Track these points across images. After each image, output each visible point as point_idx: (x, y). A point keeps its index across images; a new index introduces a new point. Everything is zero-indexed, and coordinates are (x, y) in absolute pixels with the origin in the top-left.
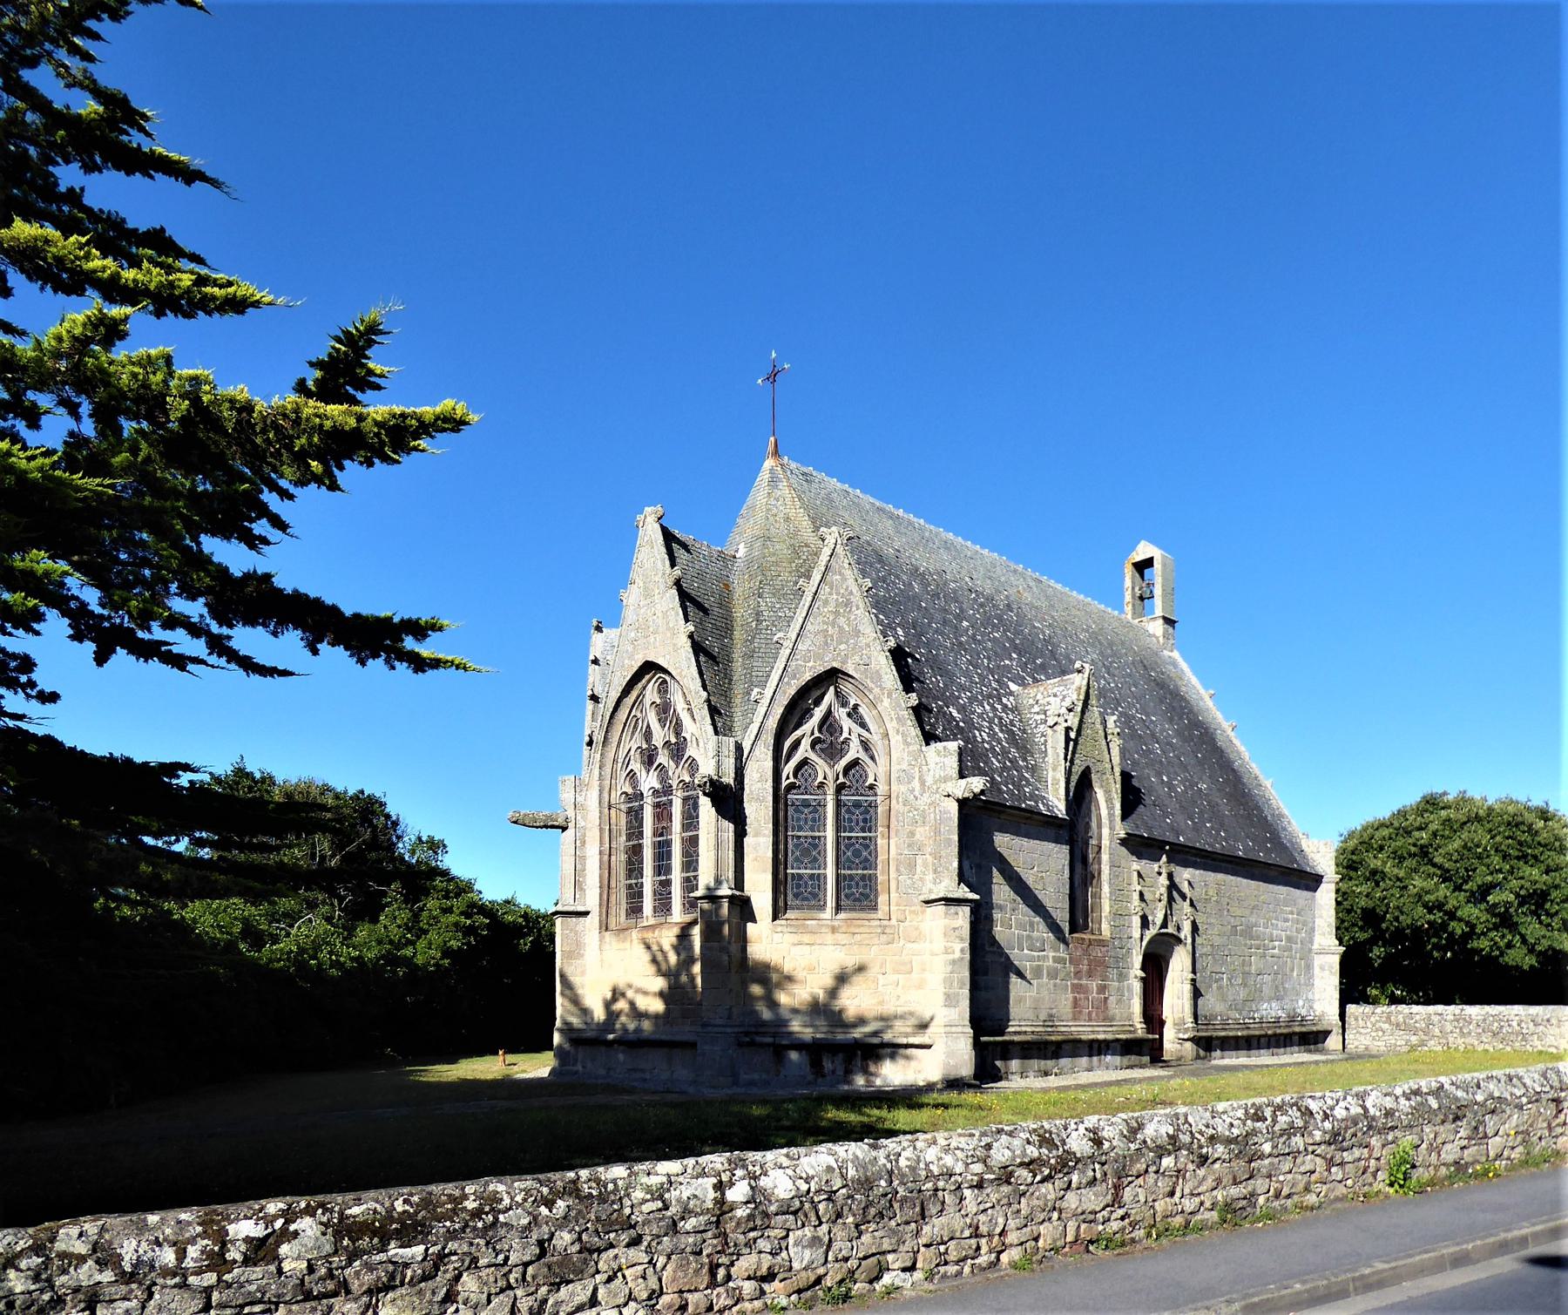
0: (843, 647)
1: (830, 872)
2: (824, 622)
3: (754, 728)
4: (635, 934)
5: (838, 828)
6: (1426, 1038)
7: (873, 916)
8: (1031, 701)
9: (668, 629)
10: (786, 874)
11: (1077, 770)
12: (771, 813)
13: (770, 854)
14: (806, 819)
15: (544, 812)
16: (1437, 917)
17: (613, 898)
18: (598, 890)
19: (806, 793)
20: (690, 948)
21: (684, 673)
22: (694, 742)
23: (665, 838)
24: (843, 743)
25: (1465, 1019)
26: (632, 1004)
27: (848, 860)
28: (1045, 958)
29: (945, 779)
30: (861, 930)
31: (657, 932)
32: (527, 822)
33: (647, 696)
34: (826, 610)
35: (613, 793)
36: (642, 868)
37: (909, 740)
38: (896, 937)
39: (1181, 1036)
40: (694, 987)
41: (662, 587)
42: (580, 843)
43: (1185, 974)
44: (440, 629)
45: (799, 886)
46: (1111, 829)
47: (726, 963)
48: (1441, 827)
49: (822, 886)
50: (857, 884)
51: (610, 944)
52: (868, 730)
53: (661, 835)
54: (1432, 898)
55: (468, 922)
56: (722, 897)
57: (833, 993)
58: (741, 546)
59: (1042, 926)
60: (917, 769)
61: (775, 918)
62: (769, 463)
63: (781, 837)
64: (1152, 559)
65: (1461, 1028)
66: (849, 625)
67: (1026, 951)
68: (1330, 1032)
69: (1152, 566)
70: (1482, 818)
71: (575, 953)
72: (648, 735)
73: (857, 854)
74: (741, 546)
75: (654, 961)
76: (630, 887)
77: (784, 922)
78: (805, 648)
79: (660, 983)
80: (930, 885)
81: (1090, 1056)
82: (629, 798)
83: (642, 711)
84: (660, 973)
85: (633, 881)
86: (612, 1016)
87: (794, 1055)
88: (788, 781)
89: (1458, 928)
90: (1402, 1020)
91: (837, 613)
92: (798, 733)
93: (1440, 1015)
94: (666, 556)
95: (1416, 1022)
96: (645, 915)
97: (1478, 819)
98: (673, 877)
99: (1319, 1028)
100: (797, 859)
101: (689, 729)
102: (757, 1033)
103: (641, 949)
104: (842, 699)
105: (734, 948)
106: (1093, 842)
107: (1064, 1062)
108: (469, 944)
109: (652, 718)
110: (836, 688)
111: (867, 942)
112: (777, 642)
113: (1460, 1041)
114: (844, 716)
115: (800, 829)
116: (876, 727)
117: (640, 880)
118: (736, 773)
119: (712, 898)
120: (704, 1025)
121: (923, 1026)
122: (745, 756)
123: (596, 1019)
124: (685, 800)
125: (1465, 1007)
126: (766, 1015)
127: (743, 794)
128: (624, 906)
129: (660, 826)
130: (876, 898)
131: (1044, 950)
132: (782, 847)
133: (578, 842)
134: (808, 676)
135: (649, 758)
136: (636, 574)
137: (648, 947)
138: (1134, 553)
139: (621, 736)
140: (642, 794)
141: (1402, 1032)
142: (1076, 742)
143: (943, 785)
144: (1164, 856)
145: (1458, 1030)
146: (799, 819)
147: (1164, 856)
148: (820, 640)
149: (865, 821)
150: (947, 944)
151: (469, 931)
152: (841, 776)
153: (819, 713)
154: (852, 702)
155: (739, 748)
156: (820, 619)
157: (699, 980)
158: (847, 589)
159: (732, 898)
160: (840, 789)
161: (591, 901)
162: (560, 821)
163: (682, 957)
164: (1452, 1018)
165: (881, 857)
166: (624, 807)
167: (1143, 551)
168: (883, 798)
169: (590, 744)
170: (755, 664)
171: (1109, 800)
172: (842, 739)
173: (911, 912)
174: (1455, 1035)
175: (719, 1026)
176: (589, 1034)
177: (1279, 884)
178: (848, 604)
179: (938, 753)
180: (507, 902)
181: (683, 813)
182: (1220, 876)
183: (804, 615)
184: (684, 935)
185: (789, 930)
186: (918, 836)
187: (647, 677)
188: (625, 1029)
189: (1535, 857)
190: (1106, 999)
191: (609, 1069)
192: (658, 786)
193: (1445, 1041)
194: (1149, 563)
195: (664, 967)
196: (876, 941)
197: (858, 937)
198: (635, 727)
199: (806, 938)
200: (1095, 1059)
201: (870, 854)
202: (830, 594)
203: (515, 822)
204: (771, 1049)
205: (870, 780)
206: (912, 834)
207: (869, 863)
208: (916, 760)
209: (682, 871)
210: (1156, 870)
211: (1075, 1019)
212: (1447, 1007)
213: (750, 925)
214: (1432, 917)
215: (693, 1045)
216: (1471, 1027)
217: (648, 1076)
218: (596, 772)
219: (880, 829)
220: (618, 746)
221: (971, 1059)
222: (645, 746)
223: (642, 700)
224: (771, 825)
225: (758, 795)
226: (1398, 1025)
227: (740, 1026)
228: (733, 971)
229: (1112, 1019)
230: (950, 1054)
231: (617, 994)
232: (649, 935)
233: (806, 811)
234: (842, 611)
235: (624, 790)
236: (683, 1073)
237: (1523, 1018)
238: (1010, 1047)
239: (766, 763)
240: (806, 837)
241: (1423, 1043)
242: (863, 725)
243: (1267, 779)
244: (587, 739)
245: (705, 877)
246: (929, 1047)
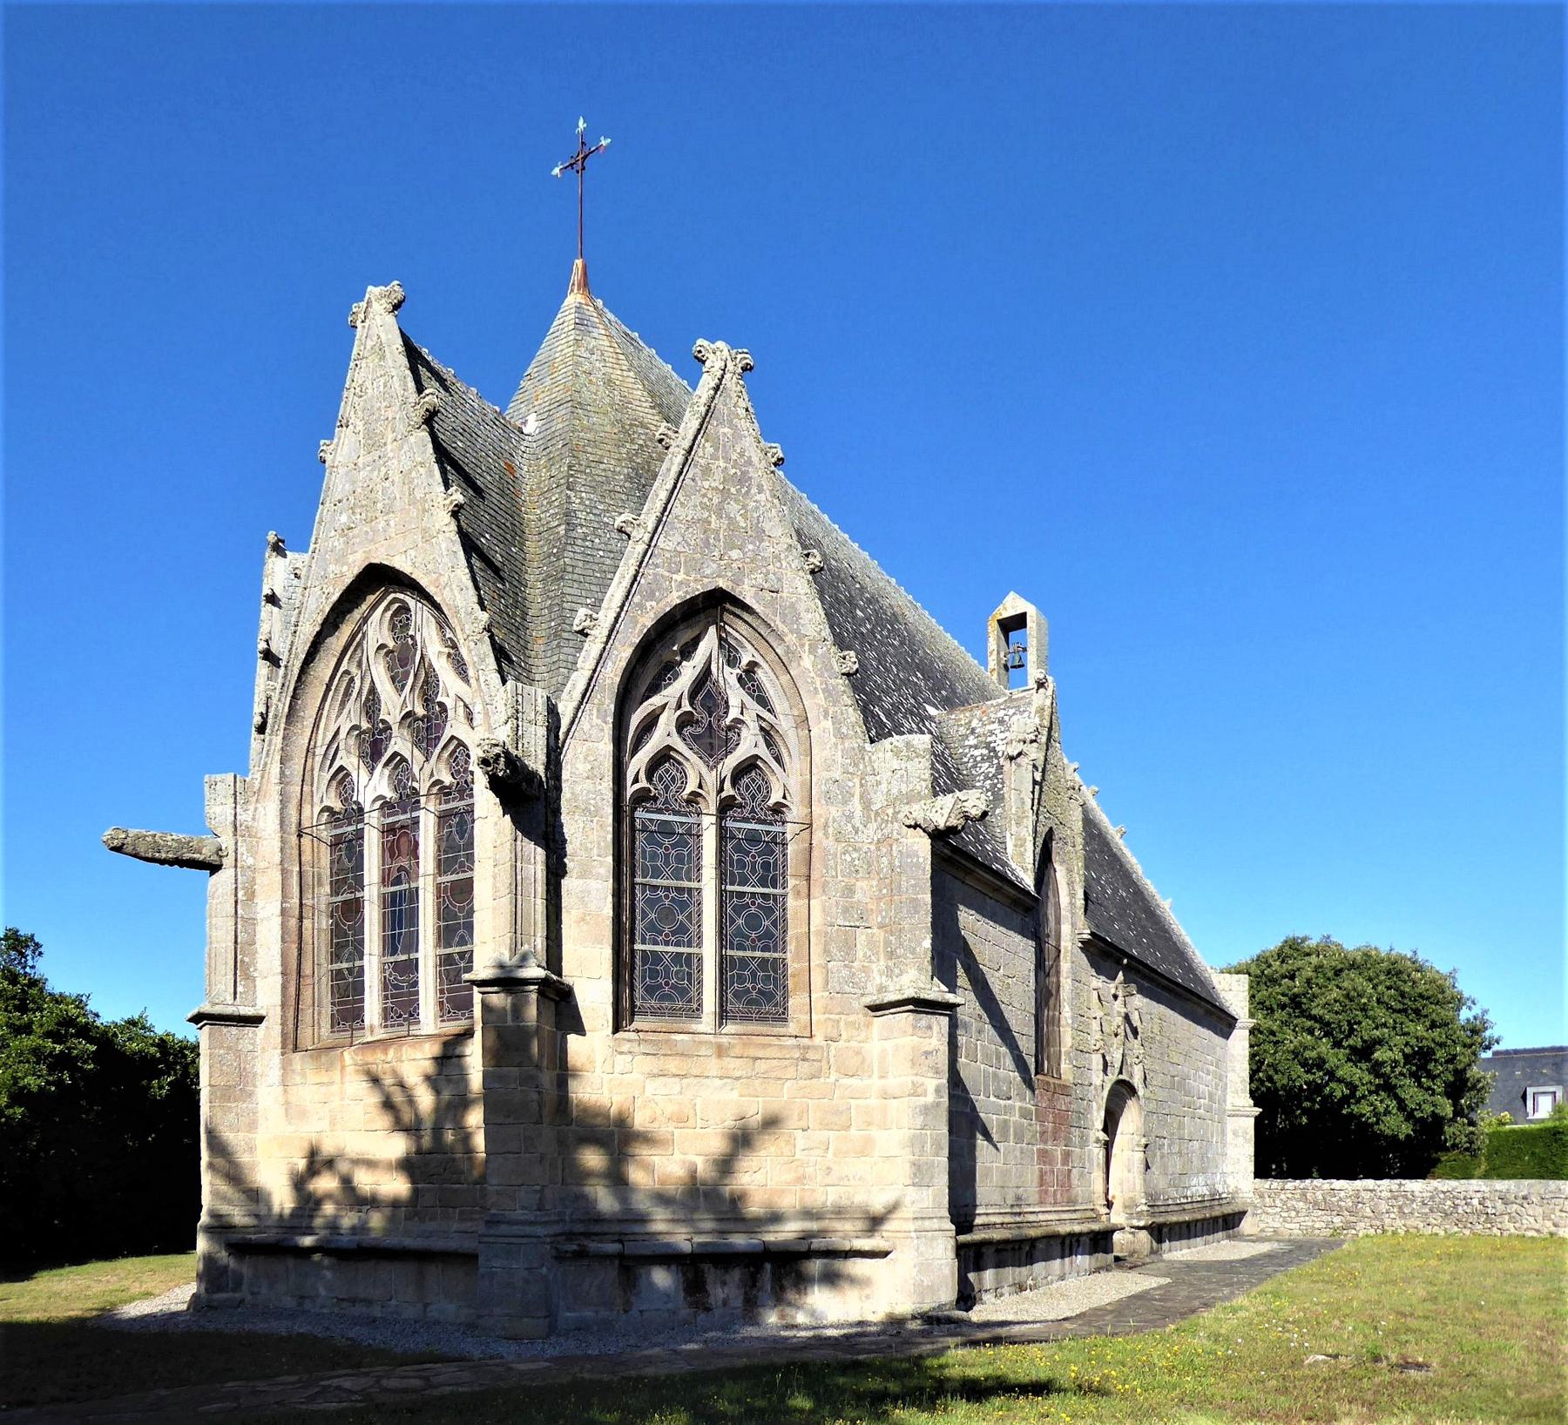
0: (735, 554)
1: (709, 951)
2: (704, 507)
3: (579, 680)
4: (348, 1056)
5: (722, 877)
6: (1353, 1219)
7: (782, 1031)
8: (962, 730)
9: (413, 503)
10: (633, 951)
11: (1043, 830)
12: (610, 837)
13: (608, 911)
14: (667, 856)
15: (173, 839)
16: (1318, 1076)
17: (307, 994)
18: (279, 979)
19: (667, 809)
20: (462, 1077)
21: (444, 580)
22: (461, 710)
23: (404, 886)
24: (729, 728)
25: (1405, 1197)
26: (347, 1182)
27: (739, 933)
28: (1008, 1110)
29: (910, 798)
30: (768, 1053)
31: (391, 1052)
32: (142, 850)
33: (370, 633)
34: (706, 484)
36: (362, 942)
37: (844, 730)
38: (825, 1067)
39: (1135, 1223)
40: (469, 1150)
41: (401, 428)
42: (243, 898)
43: (1137, 1138)
45: (654, 974)
46: (1072, 925)
47: (535, 1106)
48: (1314, 974)
49: (695, 976)
50: (754, 974)
51: (304, 1075)
52: (771, 711)
53: (398, 881)
54: (1314, 1054)
55: (58, 1048)
56: (527, 982)
57: (726, 1165)
58: (532, 418)
59: (1009, 1061)
60: (857, 780)
61: (617, 1028)
62: (574, 299)
63: (626, 884)
64: (1023, 616)
65: (1400, 1207)
66: (744, 516)
67: (992, 1098)
68: (1244, 1213)
69: (1025, 626)
70: (1362, 964)
71: (238, 1088)
72: (372, 704)
73: (753, 922)
74: (532, 418)
75: (388, 1105)
76: (338, 975)
77: (633, 1035)
78: (670, 546)
79: (397, 1146)
80: (878, 979)
81: (1062, 1257)
83: (359, 665)
84: (399, 1126)
85: (345, 965)
86: (308, 1203)
87: (661, 1278)
88: (637, 786)
89: (1339, 1091)
90: (1321, 1197)
91: (724, 492)
92: (656, 701)
93: (1371, 1191)
94: (408, 372)
95: (1341, 1199)
96: (367, 1022)
97: (1353, 966)
98: (420, 955)
99: (1228, 1210)
100: (651, 927)
101: (450, 685)
102: (587, 1235)
103: (358, 1087)
104: (731, 655)
105: (547, 1078)
106: (1052, 941)
107: (1039, 1267)
108: (59, 1083)
109: (380, 674)
110: (720, 629)
112: (620, 530)
113: (1399, 1223)
114: (733, 680)
115: (657, 873)
116: (786, 705)
117: (358, 963)
118: (548, 756)
119: (507, 982)
120: (493, 1222)
121: (875, 1222)
122: (563, 729)
123: (276, 1209)
124: (443, 818)
125: (1403, 1182)
126: (604, 1199)
127: (559, 798)
128: (327, 1010)
129: (396, 865)
130: (785, 998)
131: (1009, 1098)
132: (626, 901)
133: (240, 894)
134: (675, 598)
135: (373, 746)
136: (349, 408)
137: (375, 1080)
138: (1001, 607)
139: (321, 708)
140: (361, 810)
141: (1320, 1213)
142: (1040, 784)
143: (905, 809)
144: (1121, 973)
145: (1395, 1210)
146: (654, 856)
147: (1121, 973)
148: (695, 535)
149: (766, 866)
150: (915, 1079)
151: (61, 1062)
152: (727, 784)
153: (688, 672)
154: (745, 660)
155: (552, 711)
156: (696, 499)
157: (479, 1141)
158: (742, 454)
159: (543, 983)
160: (726, 806)
161: (267, 996)
162: (206, 854)
163: (446, 1096)
164: (1389, 1195)
165: (794, 930)
166: (326, 834)
167: (1013, 605)
168: (797, 828)
169: (261, 729)
170: (568, 590)
171: (1070, 884)
172: (728, 721)
173: (847, 1024)
174: (1392, 1216)
175: (524, 1223)
176: (269, 1236)
177: (1203, 1026)
178: (743, 479)
179: (896, 753)
180: (132, 1023)
181: (439, 840)
182: (1162, 1008)
183: (669, 486)
184: (449, 1057)
185: (644, 1048)
186: (858, 896)
187: (371, 599)
188: (333, 1226)
189: (1417, 1012)
190: (1070, 1171)
191: (303, 1297)
192: (389, 794)
193: (1378, 1223)
194: (1019, 621)
195: (407, 1116)
197: (762, 1066)
198: (347, 694)
199: (673, 1065)
200: (1067, 1260)
201: (774, 924)
203: (118, 849)
205: (776, 797)
206: (849, 891)
207: (773, 938)
208: (856, 765)
209: (438, 945)
210: (1113, 991)
211: (1041, 1203)
212: (1378, 1182)
213: (572, 1039)
214: (1311, 1077)
215: (470, 1258)
216: (1414, 1206)
217: (377, 1311)
218: (275, 769)
219: (791, 882)
220: (316, 725)
221: (953, 1274)
222: (365, 725)
223: (360, 644)
224: (610, 859)
225: (587, 802)
226: (1316, 1203)
227: (557, 1222)
228: (546, 1120)
229: (1074, 1202)
230: (923, 1267)
231: (317, 1162)
232: (381, 1061)
233: (667, 842)
234: (733, 490)
235: (325, 804)
236: (446, 1308)
237: (1487, 1195)
238: (984, 1250)
239: (601, 745)
240: (667, 889)
241: (1348, 1226)
242: (763, 701)
243: (1165, 899)
244: (257, 720)
245: (488, 954)
246: (884, 1254)
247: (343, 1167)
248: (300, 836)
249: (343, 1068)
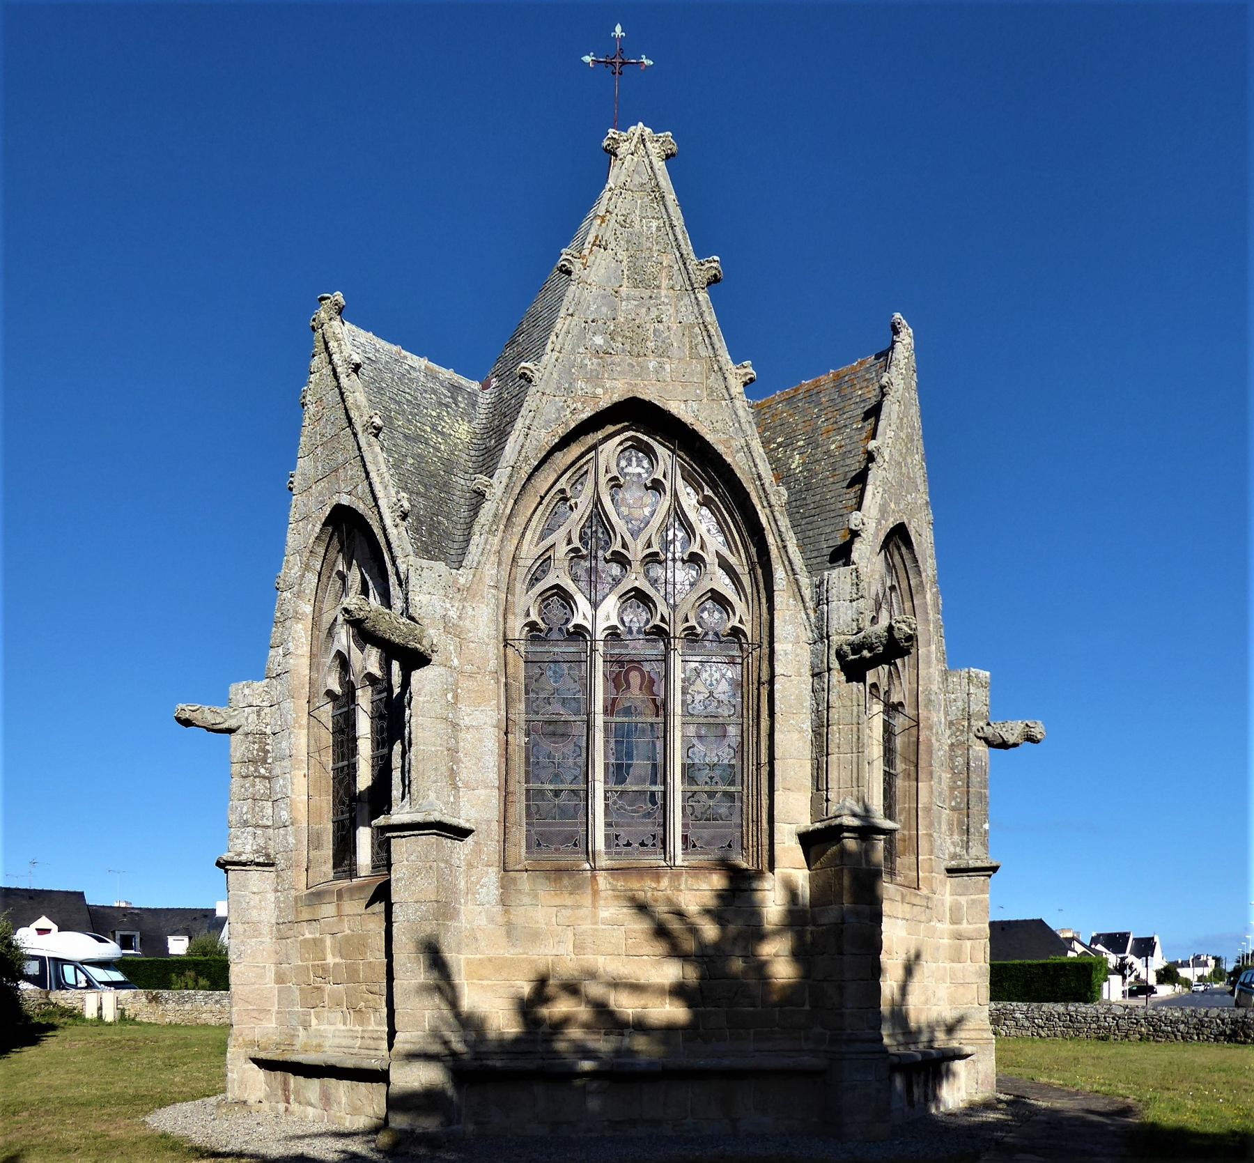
75: (661, 932)
84: (676, 952)
137: (642, 908)
187: (610, 429)
195: (689, 945)
247: (594, 990)
248: (505, 646)
249: (595, 893)
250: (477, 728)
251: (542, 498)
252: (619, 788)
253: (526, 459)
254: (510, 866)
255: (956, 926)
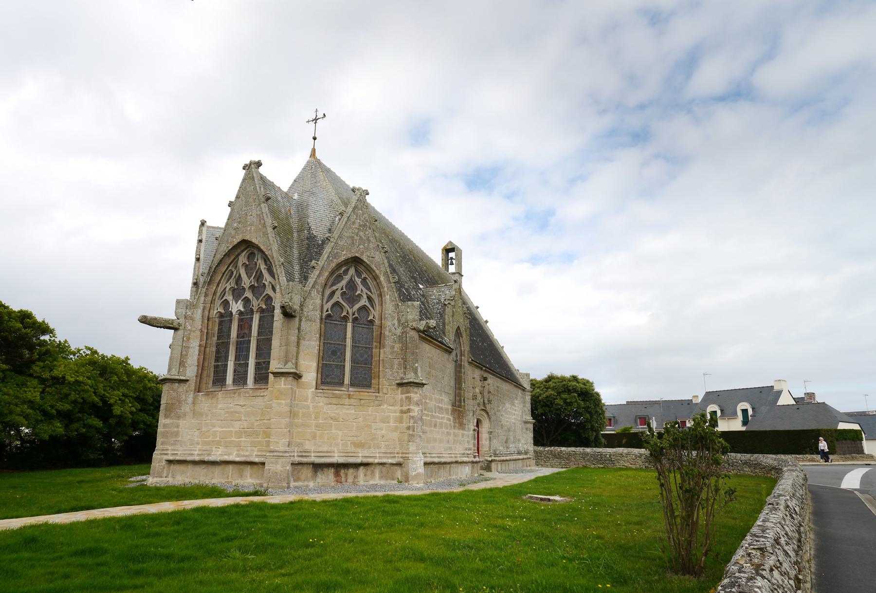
2: (353, 233)
35: (212, 311)
44: (307, 122)
52: (371, 292)
66: (365, 236)
72: (239, 279)
82: (221, 315)
88: (327, 313)
92: (334, 288)
111: (367, 405)
148: (350, 242)
152: (356, 313)
153: (347, 278)
196: (372, 404)
197: (362, 402)
202: (356, 219)
204: (311, 466)
209: (256, 359)
219: (375, 344)
242: (369, 289)
249: (218, 399)
250: (194, 347)
251: (224, 274)
252: (238, 362)
253: (214, 264)
254: (706, 376)
255: (401, 408)
